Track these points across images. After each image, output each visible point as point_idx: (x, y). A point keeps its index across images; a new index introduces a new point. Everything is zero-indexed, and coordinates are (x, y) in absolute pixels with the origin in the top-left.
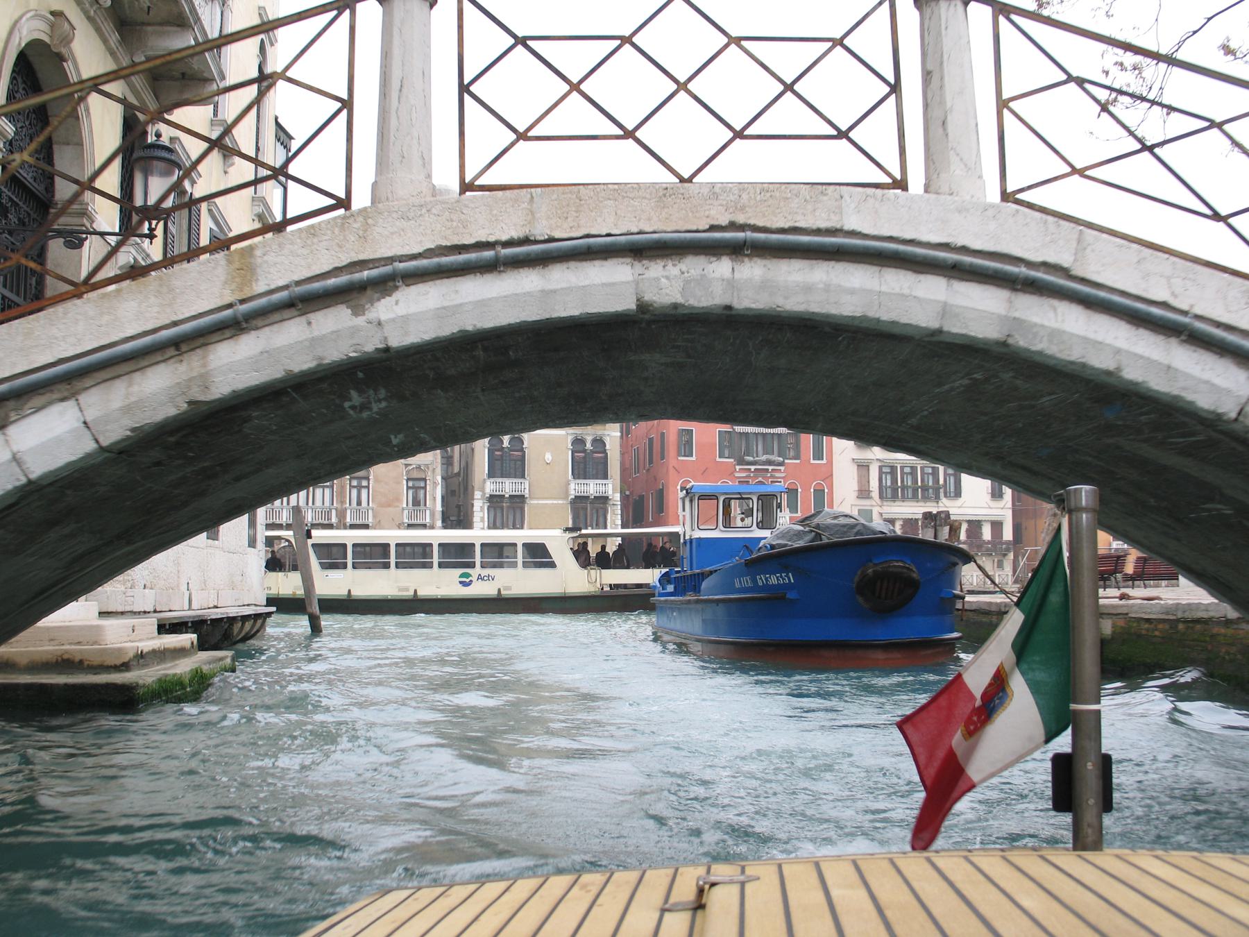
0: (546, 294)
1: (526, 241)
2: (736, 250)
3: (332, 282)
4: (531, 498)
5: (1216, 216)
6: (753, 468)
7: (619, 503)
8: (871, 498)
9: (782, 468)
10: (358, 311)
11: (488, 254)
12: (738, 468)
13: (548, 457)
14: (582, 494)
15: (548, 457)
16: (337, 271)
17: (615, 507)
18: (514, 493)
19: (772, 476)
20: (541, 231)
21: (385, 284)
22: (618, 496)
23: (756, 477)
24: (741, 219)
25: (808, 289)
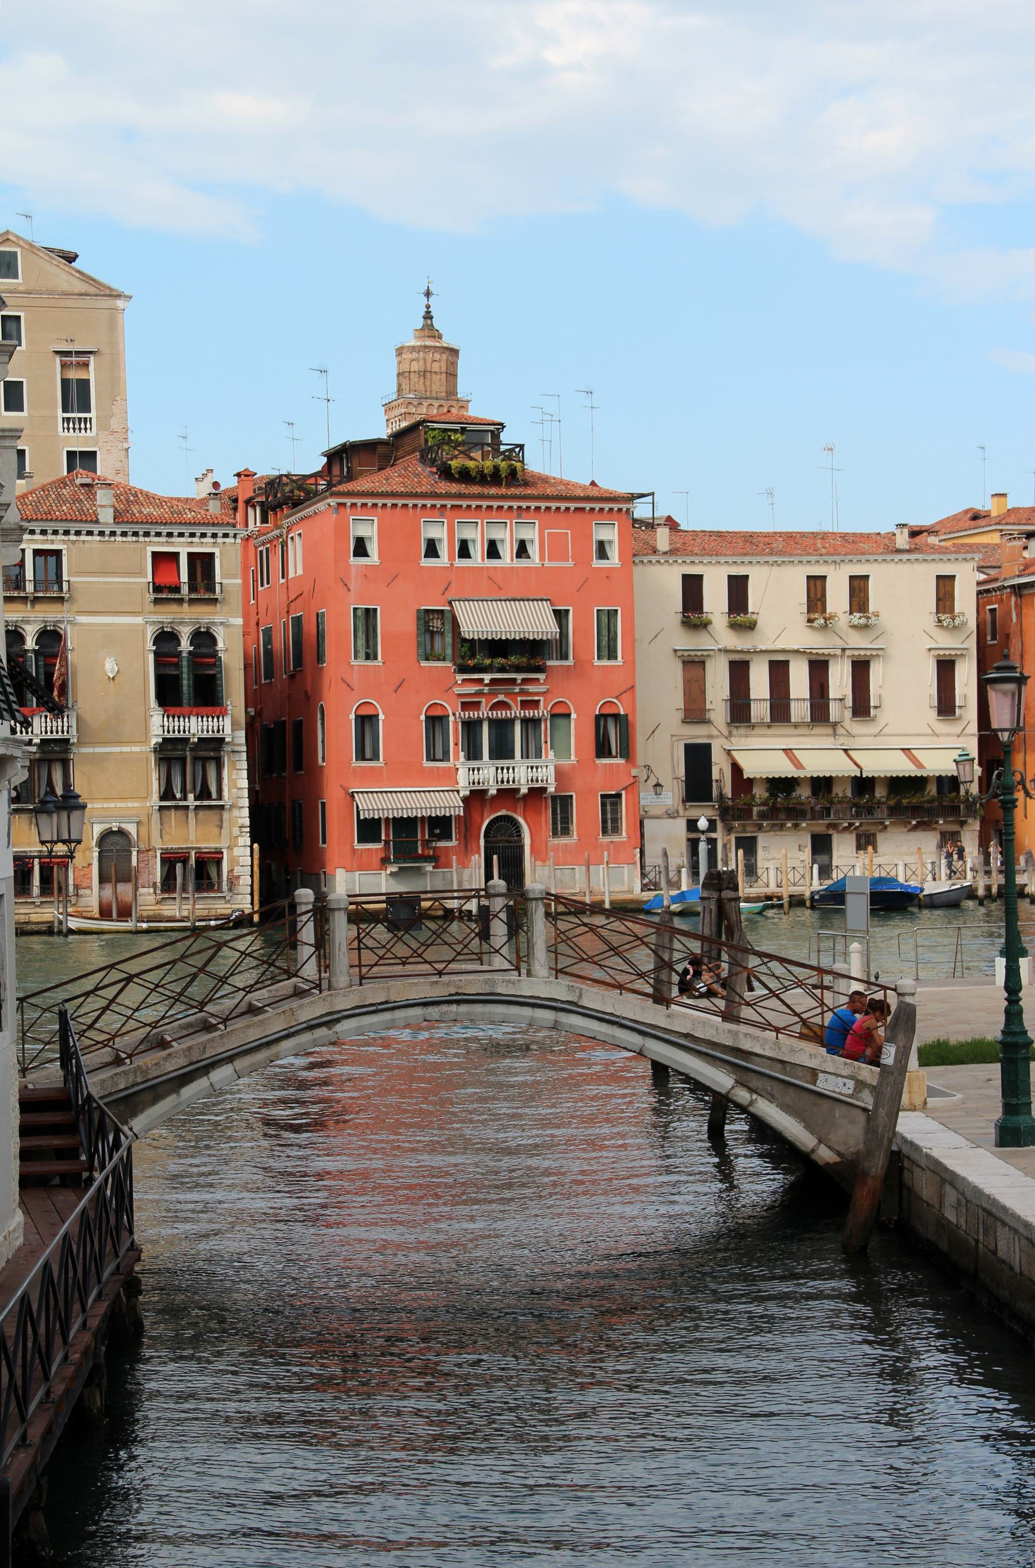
0: (406, 1018)
1: (386, 1002)
2: (458, 1002)
4: (80, 743)
6: (487, 677)
7: (244, 748)
8: (708, 722)
9: (541, 677)
10: (330, 1029)
11: (374, 1008)
12: (460, 678)
13: (110, 666)
14: (177, 735)
15: (110, 666)
16: (322, 1016)
17: (237, 757)
18: (49, 736)
19: (523, 692)
20: (392, 998)
21: (338, 1021)
22: (241, 736)
23: (493, 694)
24: (460, 991)
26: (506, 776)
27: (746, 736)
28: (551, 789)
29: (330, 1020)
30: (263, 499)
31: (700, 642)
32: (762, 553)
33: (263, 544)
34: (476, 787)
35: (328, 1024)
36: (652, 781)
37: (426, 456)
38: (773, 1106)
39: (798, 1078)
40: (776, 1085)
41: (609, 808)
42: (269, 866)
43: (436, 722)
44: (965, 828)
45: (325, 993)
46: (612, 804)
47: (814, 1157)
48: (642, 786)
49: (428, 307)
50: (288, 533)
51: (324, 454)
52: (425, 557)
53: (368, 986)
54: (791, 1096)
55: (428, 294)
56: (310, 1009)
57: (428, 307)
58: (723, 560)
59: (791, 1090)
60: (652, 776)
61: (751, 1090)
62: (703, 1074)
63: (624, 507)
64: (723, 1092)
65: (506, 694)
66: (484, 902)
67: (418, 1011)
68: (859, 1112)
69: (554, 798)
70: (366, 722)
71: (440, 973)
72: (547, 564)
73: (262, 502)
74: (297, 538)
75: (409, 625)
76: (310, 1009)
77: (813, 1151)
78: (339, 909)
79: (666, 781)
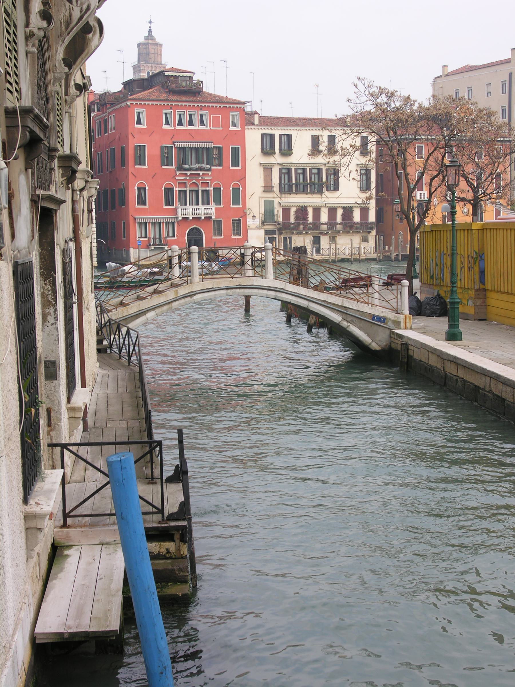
1: (213, 288)
2: (239, 288)
3: (189, 295)
5: (386, 301)
9: (210, 173)
19: (202, 179)
21: (195, 295)
23: (191, 179)
25: (249, 292)
26: (196, 212)
27: (287, 197)
28: (213, 217)
29: (191, 295)
30: (98, 101)
31: (271, 160)
32: (293, 126)
33: (98, 119)
34: (185, 216)
35: (191, 296)
36: (252, 215)
37: (164, 86)
38: (356, 328)
39: (365, 317)
40: (356, 319)
41: (235, 225)
42: (101, 247)
43: (169, 191)
44: (370, 234)
45: (189, 285)
46: (237, 223)
47: (370, 347)
48: (248, 217)
49: (150, 27)
50: (109, 115)
51: (123, 84)
52: (178, 125)
53: (206, 282)
54: (362, 324)
55: (150, 22)
56: (182, 291)
57: (150, 27)
58: (279, 128)
59: (363, 321)
60: (251, 213)
61: (348, 322)
62: (331, 316)
63: (242, 106)
64: (338, 322)
65: (196, 180)
66: (243, 251)
67: (224, 292)
68: (387, 330)
69: (214, 221)
70: (141, 190)
71: (232, 278)
72: (212, 128)
73: (98, 103)
74: (113, 118)
75: (157, 152)
76: (182, 291)
77: (370, 344)
78: (195, 252)
79: (257, 215)
